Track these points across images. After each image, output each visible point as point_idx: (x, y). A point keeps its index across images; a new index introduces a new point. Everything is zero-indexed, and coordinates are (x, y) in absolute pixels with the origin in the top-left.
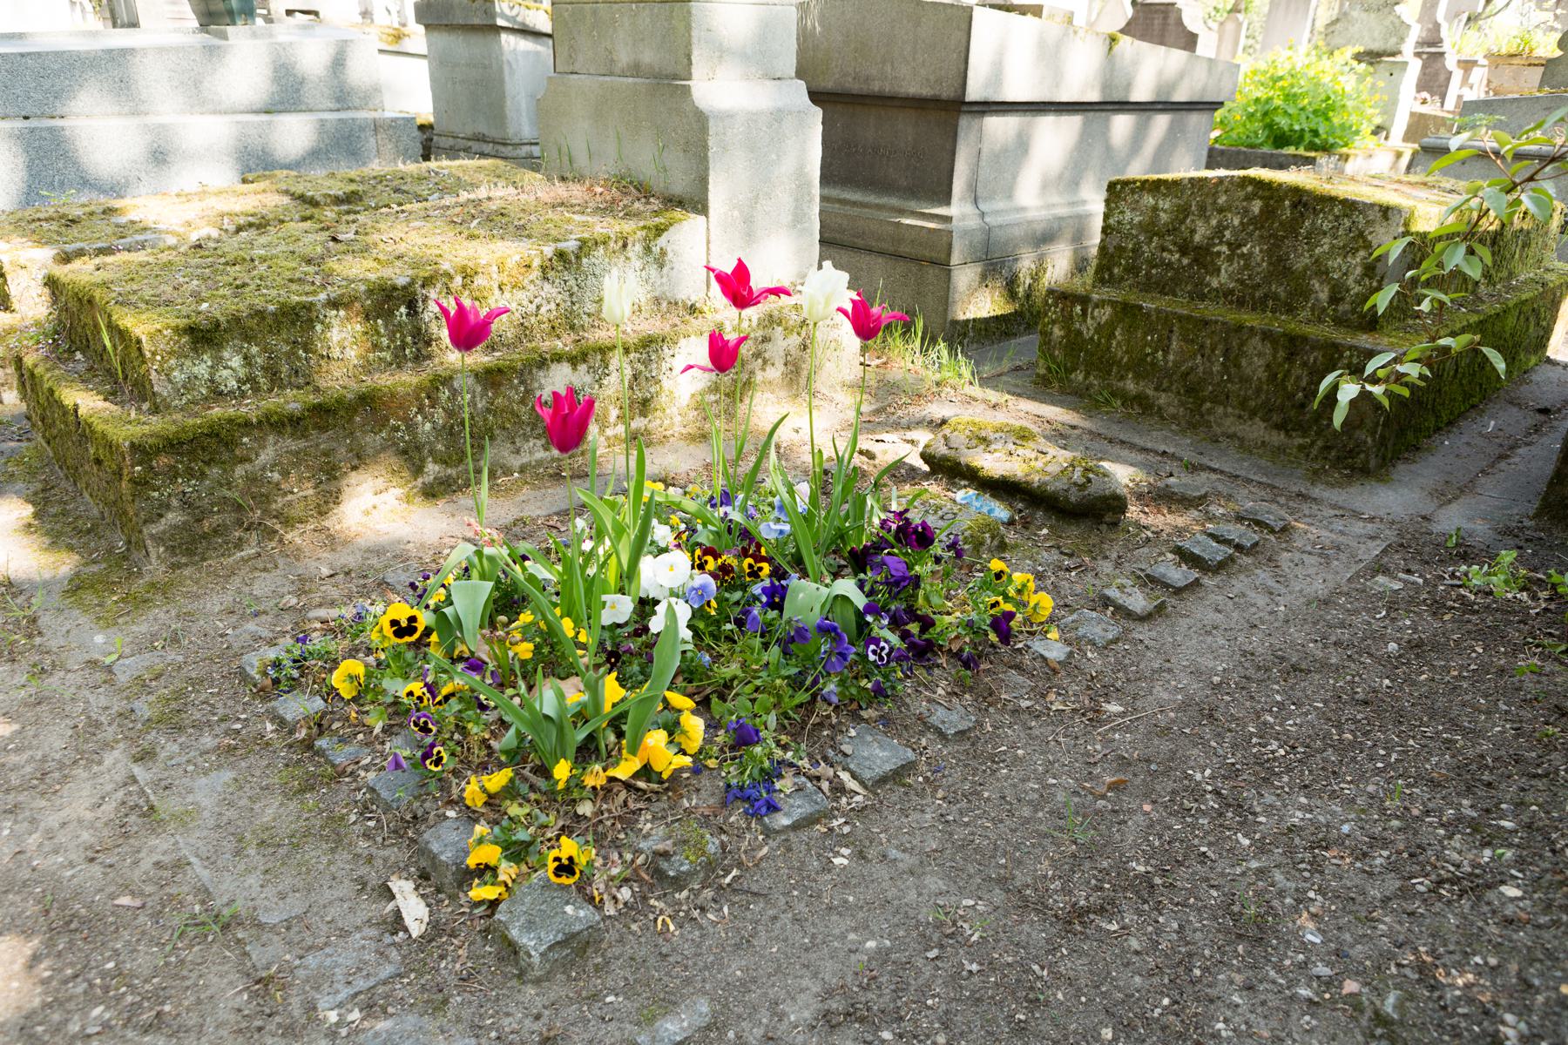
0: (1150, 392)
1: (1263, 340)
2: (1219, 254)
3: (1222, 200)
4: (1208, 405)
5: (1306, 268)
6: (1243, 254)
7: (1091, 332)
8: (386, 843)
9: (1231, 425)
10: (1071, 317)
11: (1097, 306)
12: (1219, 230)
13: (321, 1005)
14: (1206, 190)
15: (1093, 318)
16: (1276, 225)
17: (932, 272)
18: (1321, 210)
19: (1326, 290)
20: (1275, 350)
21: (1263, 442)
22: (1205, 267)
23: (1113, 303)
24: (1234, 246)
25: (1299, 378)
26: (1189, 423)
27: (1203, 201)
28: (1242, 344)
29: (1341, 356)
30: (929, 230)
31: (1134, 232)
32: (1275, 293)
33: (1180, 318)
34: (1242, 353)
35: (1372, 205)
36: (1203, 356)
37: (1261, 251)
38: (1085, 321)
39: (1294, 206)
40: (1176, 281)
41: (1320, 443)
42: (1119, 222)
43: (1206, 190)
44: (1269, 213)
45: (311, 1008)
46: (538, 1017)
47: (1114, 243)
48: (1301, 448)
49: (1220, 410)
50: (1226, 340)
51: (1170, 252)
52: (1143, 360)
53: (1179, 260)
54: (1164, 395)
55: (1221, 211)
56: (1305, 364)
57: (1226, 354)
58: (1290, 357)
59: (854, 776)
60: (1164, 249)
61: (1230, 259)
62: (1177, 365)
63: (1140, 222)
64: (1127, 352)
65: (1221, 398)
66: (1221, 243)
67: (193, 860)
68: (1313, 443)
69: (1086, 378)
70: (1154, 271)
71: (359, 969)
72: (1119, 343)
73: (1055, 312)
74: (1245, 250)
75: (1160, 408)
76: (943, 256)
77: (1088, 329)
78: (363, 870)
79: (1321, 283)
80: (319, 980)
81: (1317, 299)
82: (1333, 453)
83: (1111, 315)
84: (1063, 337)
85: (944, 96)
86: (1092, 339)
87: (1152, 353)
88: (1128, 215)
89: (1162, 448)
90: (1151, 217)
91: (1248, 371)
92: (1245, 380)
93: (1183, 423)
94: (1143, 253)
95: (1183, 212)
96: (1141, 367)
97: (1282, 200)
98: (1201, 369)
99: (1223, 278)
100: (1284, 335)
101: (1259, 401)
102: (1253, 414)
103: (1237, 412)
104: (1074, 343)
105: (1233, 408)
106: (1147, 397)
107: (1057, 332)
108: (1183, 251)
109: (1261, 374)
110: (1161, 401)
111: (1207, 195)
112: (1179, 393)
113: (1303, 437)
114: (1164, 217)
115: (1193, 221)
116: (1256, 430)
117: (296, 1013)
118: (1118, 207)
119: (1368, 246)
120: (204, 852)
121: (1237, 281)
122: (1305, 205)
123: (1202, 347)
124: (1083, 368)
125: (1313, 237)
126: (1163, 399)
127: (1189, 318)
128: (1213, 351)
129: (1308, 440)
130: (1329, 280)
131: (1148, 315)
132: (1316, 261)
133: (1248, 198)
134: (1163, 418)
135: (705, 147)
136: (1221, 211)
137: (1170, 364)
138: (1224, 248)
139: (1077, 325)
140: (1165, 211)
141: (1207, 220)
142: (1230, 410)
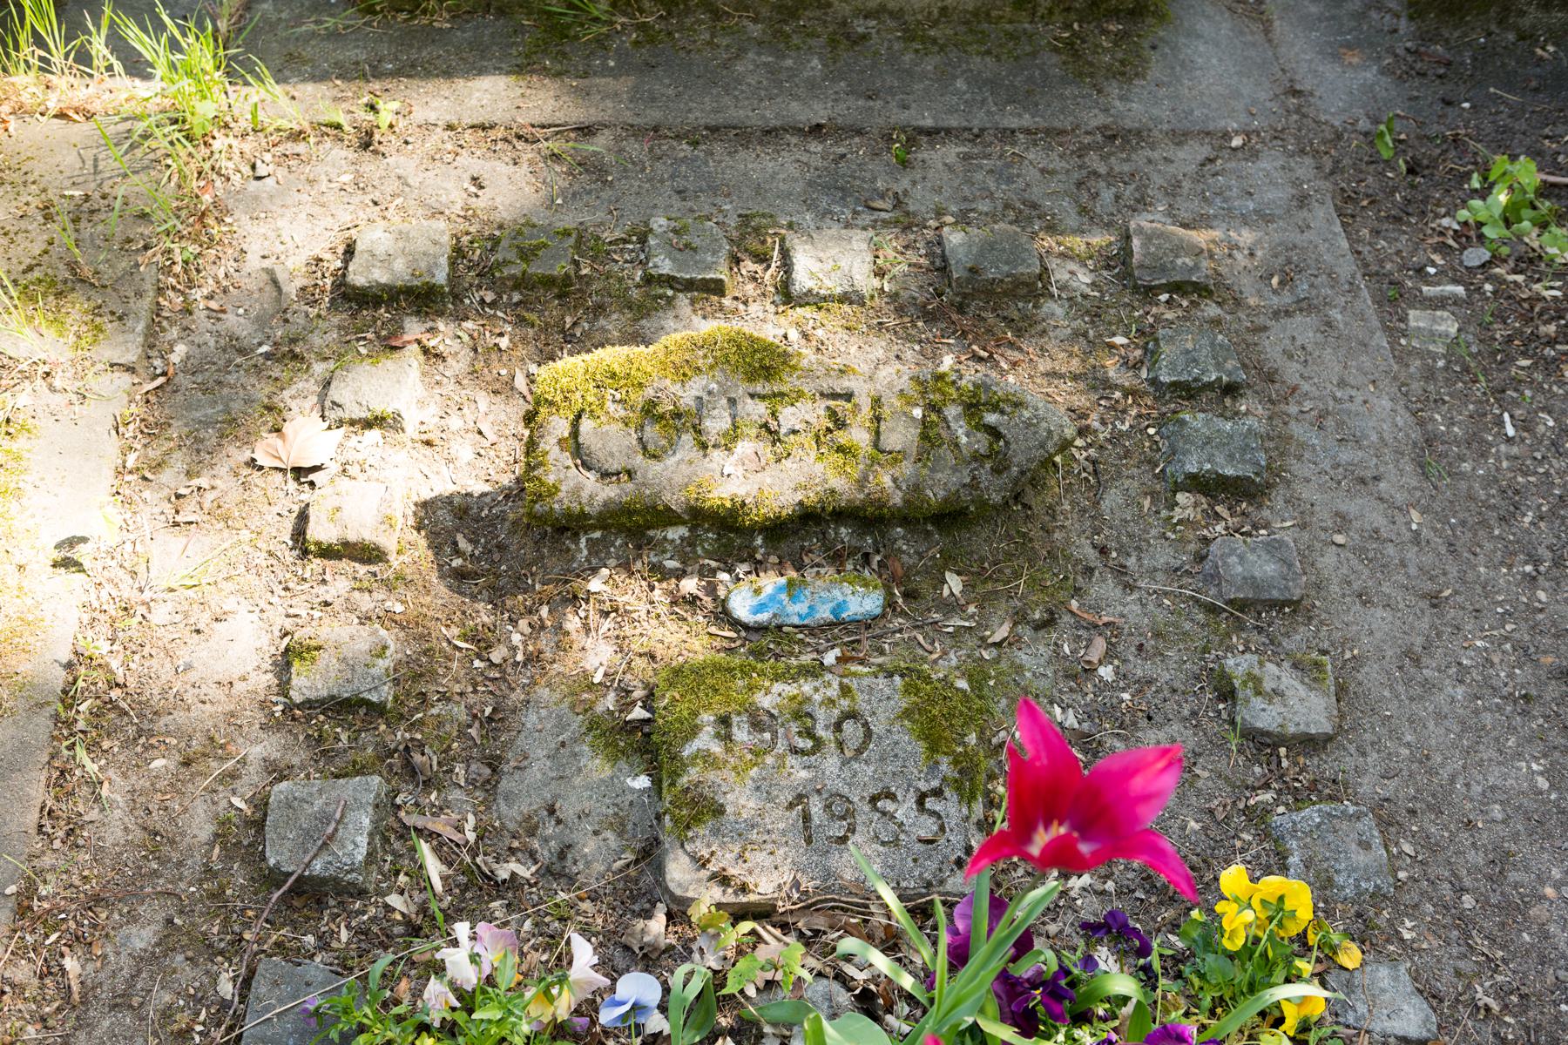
89: (819, 112)
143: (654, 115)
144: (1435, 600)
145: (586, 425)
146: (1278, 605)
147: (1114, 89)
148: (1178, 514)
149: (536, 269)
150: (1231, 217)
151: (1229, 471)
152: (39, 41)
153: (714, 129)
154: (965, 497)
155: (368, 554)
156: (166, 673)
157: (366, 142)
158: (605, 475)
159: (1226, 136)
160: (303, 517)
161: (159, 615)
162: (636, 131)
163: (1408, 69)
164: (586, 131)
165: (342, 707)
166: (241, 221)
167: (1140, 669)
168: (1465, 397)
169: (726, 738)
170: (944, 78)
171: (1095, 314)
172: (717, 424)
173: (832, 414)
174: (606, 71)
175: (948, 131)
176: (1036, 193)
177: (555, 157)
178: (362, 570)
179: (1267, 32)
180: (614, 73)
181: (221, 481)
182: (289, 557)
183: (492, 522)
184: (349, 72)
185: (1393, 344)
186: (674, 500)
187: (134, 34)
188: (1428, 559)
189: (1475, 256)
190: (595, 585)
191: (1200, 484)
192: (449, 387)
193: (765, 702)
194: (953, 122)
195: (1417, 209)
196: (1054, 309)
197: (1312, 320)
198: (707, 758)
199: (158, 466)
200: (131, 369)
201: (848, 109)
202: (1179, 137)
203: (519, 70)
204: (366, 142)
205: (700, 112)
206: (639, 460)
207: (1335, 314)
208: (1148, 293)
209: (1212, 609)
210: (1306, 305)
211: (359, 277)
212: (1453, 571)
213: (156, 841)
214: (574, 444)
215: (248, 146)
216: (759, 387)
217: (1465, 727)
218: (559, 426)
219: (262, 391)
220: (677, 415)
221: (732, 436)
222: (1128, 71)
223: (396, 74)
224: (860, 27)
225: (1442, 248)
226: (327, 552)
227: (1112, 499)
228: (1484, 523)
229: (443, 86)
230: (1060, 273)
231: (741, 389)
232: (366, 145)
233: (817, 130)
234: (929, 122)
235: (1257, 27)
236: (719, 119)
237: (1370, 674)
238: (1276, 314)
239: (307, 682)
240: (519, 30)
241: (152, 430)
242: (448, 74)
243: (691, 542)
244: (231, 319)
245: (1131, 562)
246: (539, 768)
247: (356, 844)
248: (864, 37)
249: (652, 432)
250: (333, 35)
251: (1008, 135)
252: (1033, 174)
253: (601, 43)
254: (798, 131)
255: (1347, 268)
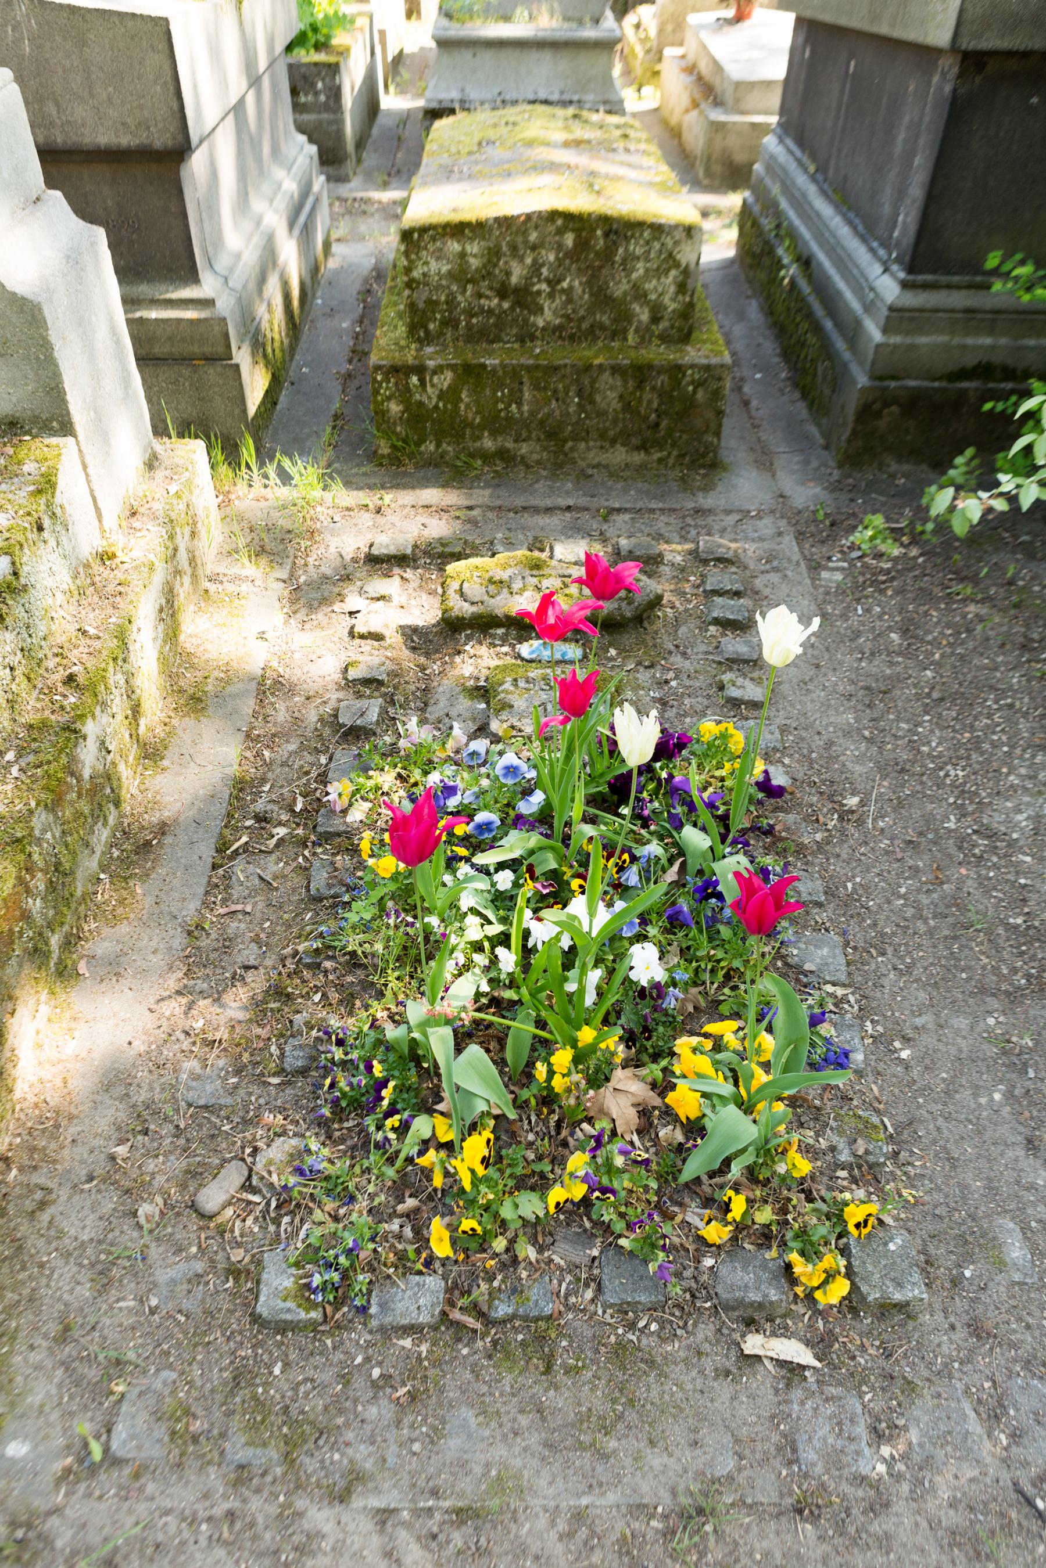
0: (510, 445)
1: (613, 374)
2: (539, 292)
3: (533, 236)
4: (570, 444)
5: (625, 293)
6: (563, 291)
7: (434, 400)
8: (690, 1328)
9: (595, 456)
10: (408, 389)
11: (434, 373)
12: (536, 267)
13: (865, 1470)
14: (514, 228)
15: (433, 386)
16: (592, 256)
17: (212, 373)
18: (632, 236)
19: (646, 311)
20: (625, 381)
21: (626, 465)
22: (527, 308)
23: (453, 367)
24: (553, 283)
25: (650, 402)
26: (555, 464)
27: (513, 241)
28: (593, 382)
29: (684, 375)
30: (191, 322)
31: (444, 282)
32: (600, 322)
33: (529, 369)
34: (593, 390)
35: (676, 226)
36: (557, 400)
37: (581, 283)
38: (424, 389)
39: (606, 235)
40: (500, 326)
41: (675, 453)
42: (424, 275)
43: (514, 228)
44: (582, 245)
45: (862, 1480)
46: (953, 1327)
47: (424, 297)
48: (660, 461)
49: (582, 446)
50: (577, 381)
51: (488, 297)
52: (496, 417)
53: (499, 305)
54: (524, 445)
55: (534, 248)
56: (653, 388)
57: (579, 393)
58: (640, 386)
59: (834, 984)
60: (480, 296)
61: (551, 296)
62: (532, 413)
63: (449, 272)
64: (477, 412)
65: (581, 435)
66: (539, 281)
67: (584, 1501)
68: (669, 454)
69: (438, 446)
70: (474, 321)
71: (839, 1424)
72: (467, 406)
73: (387, 388)
74: (565, 284)
75: (523, 457)
76: (220, 349)
77: (430, 397)
78: (708, 1365)
79: (641, 306)
80: (834, 1459)
81: (640, 322)
82: (687, 458)
83: (453, 380)
84: (403, 413)
85: (158, 144)
86: (436, 407)
87: (506, 408)
88: (434, 266)
89: (570, 502)
90: (460, 265)
91: (603, 405)
92: (601, 414)
93: (549, 465)
94: (459, 303)
95: (493, 254)
96: (496, 424)
97: (593, 230)
98: (557, 413)
99: (548, 315)
100: (632, 366)
101: (618, 430)
102: (613, 442)
103: (598, 444)
104: (417, 415)
105: (595, 441)
106: (508, 451)
107: (394, 408)
108: (502, 293)
109: (616, 405)
110: (523, 451)
111: (517, 233)
112: (539, 439)
113: (661, 451)
114: (474, 263)
115: (506, 263)
116: (619, 455)
117: (860, 1493)
118: (420, 259)
119: (677, 265)
120: (582, 1487)
121: (562, 316)
122: (616, 233)
123: (555, 391)
124: (432, 437)
125: (629, 261)
126: (524, 449)
127: (537, 367)
128: (567, 393)
129: (665, 453)
130: (648, 302)
131: (494, 371)
132: (634, 285)
133: (560, 232)
134: (528, 467)
135: (46, 346)
136: (534, 248)
137: (526, 415)
138: (544, 286)
139: (418, 397)
140: (475, 256)
141: (522, 259)
142: (591, 443)
143: (499, 503)
144: (817, 666)
145: (466, 585)
146: (746, 662)
147: (700, 494)
148: (709, 634)
149: (447, 550)
150: (746, 539)
151: (731, 617)
152: (248, 466)
153: (525, 508)
154: (616, 613)
155: (378, 637)
156: (299, 674)
157: (378, 511)
158: (473, 603)
159: (749, 512)
160: (352, 627)
161: (296, 656)
162: (491, 509)
163: (835, 488)
164: (470, 508)
165: (367, 682)
166: (327, 537)
167: (688, 683)
168: (842, 601)
169: (516, 686)
170: (625, 490)
171: (683, 570)
172: (517, 585)
173: (564, 583)
174: (479, 487)
175: (626, 509)
176: (662, 531)
177: (458, 518)
178: (376, 643)
179: (773, 476)
180: (483, 488)
181: (320, 616)
182: (347, 639)
183: (427, 633)
184: (371, 487)
185: (813, 583)
186: (499, 612)
187: (286, 463)
188: (816, 652)
189: (855, 554)
190: (467, 648)
191: (716, 621)
192: (411, 591)
193: (531, 675)
194: (628, 506)
195: (832, 538)
196: (665, 570)
197: (779, 574)
198: (506, 692)
199: (295, 612)
200: (284, 582)
201: (583, 501)
202: (728, 512)
203: (443, 486)
204: (378, 511)
205: (519, 501)
206: (486, 598)
207: (789, 573)
208: (705, 562)
209: (720, 663)
210: (776, 570)
211: (375, 551)
212: (827, 656)
213: (297, 720)
214: (461, 592)
215: (330, 512)
216: (534, 572)
217: (822, 704)
218: (456, 585)
219: (336, 590)
220: (501, 582)
221: (523, 590)
222: (707, 488)
223: (391, 488)
224: (590, 471)
225: (842, 552)
226: (362, 637)
227: (683, 630)
228: (843, 641)
229: (411, 492)
230: (668, 557)
231: (528, 572)
232: (378, 512)
233: (569, 508)
234: (617, 505)
235: (769, 474)
236: (527, 504)
237: (785, 688)
238: (762, 572)
239: (353, 674)
240: (443, 473)
241: (292, 602)
242: (413, 488)
243: (506, 635)
244: (323, 569)
245: (689, 651)
246: (443, 703)
247: (373, 715)
248: (592, 476)
249: (491, 588)
250: (365, 474)
251: (652, 511)
252: (661, 525)
253: (478, 478)
254: (561, 509)
255: (796, 556)
